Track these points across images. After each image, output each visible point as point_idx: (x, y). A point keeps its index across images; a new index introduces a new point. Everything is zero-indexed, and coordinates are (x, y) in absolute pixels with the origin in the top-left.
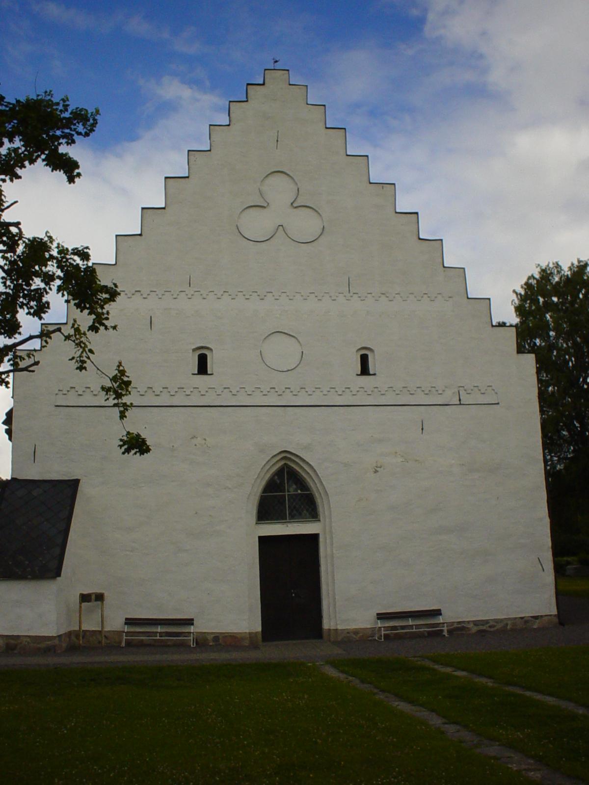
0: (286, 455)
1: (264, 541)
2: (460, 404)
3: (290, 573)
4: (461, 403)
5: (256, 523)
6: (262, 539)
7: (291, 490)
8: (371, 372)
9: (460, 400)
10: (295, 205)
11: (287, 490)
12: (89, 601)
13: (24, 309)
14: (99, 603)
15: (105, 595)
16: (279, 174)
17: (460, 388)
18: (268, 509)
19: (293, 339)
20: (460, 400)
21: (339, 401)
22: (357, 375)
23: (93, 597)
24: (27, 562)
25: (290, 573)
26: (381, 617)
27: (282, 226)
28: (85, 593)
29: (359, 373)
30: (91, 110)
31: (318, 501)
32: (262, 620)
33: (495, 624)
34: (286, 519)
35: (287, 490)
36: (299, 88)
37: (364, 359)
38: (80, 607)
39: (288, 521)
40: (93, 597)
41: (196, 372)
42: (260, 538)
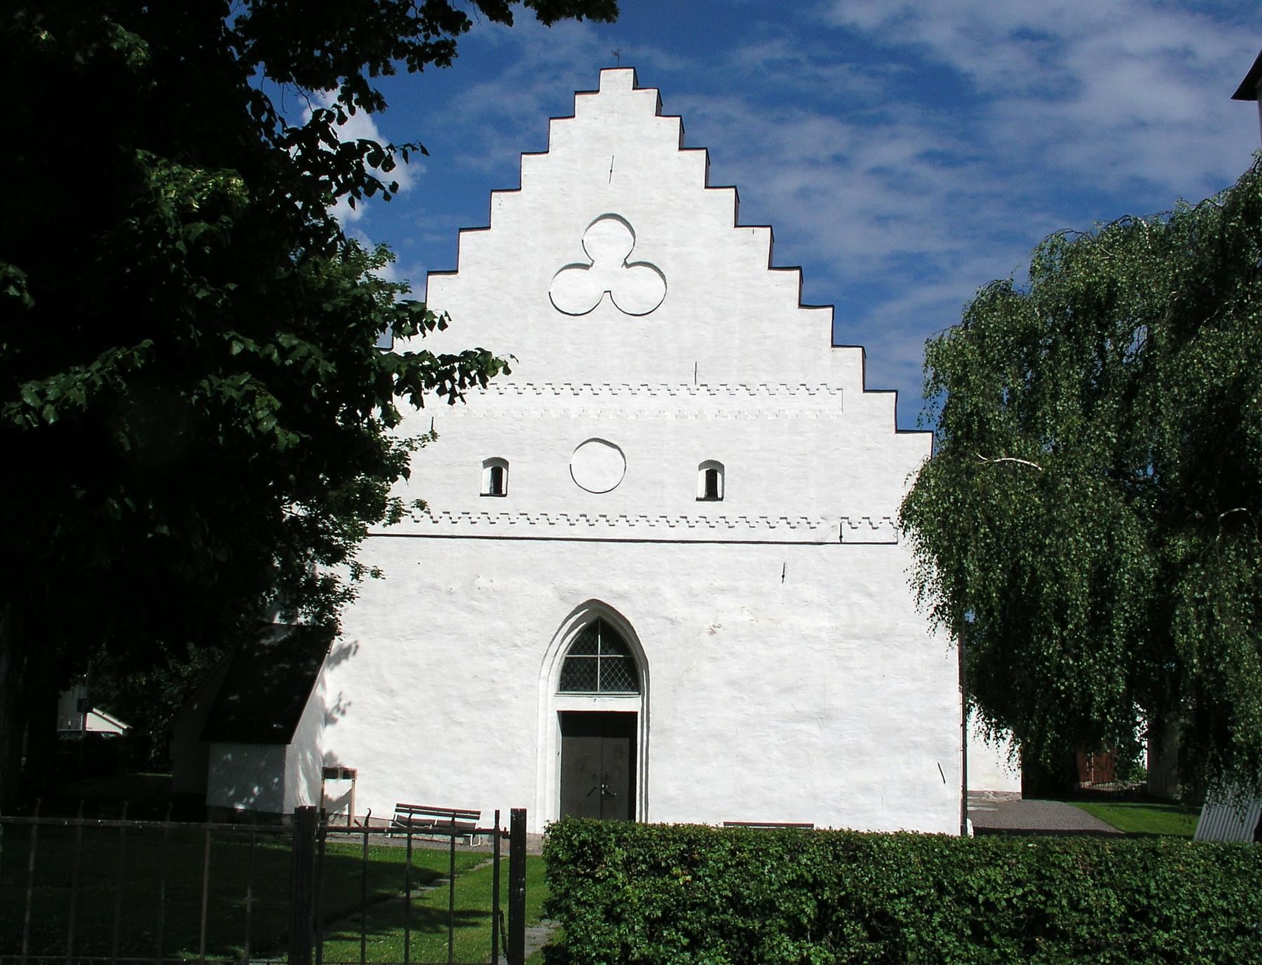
3: (601, 753)
10: (629, 261)
11: (603, 648)
25: (601, 753)
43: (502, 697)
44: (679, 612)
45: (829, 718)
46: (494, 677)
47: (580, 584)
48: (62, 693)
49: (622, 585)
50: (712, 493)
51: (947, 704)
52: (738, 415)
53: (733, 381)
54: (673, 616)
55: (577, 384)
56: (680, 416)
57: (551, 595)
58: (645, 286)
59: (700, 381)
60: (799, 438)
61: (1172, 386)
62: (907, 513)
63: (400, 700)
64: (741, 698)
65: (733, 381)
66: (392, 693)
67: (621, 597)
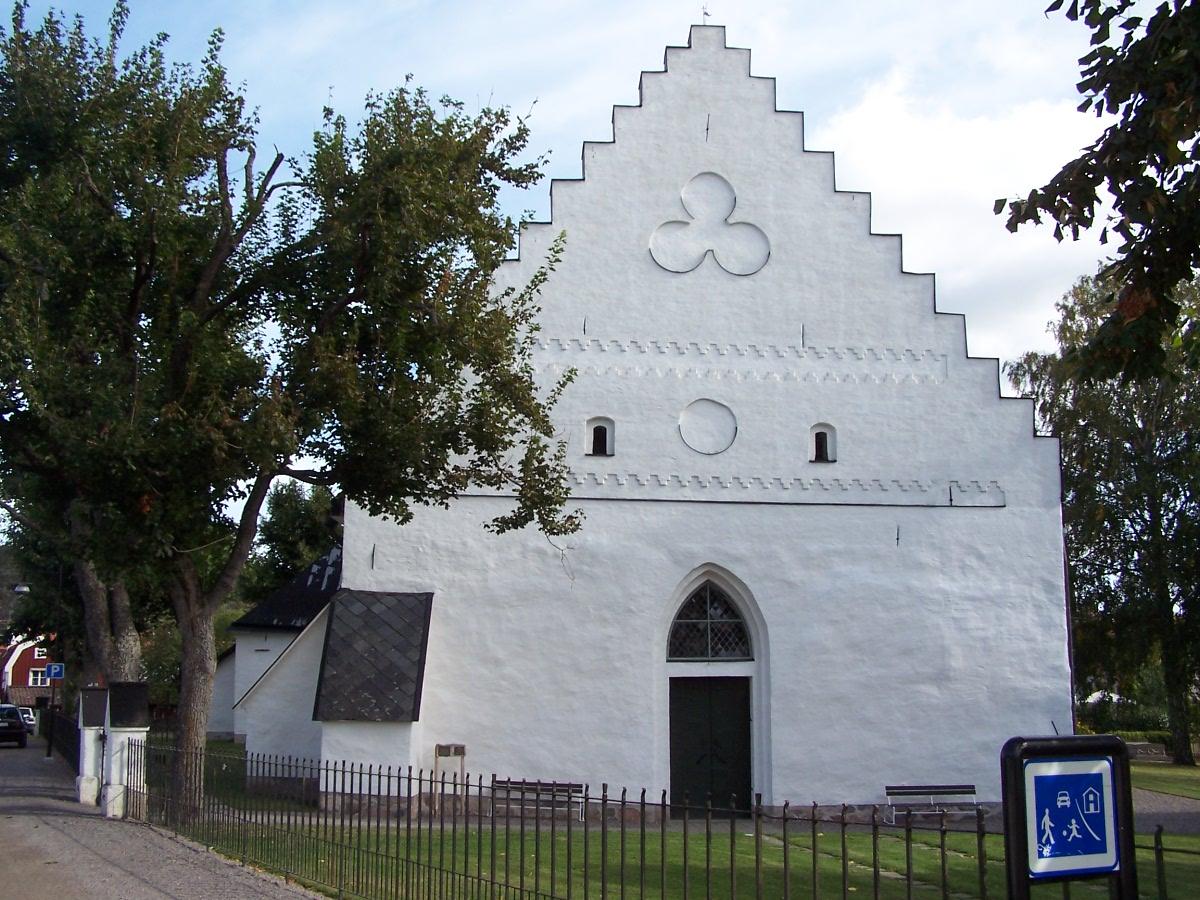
0: (710, 568)
1: (675, 683)
2: (951, 506)
3: (713, 733)
4: (954, 504)
5: (668, 661)
6: (674, 681)
7: (715, 613)
8: (830, 458)
9: (951, 500)
10: (731, 221)
11: (712, 618)
12: (448, 755)
13: (1037, 221)
14: (459, 758)
15: (467, 748)
16: (713, 179)
17: (952, 484)
18: (682, 643)
19: (724, 409)
20: (951, 500)
21: (785, 497)
22: (811, 461)
23: (453, 750)
24: (374, 701)
25: (713, 733)
26: (891, 791)
27: (712, 251)
28: (443, 743)
29: (814, 459)
30: (319, 124)
31: (753, 632)
32: (1036, 790)
33: (988, 809)
34: (707, 656)
35: (712, 618)
36: (740, 53)
37: (821, 440)
38: (436, 762)
39: (710, 658)
40: (453, 750)
41: (591, 452)
42: (672, 680)
43: (618, 665)
44: (797, 574)
45: (948, 679)
46: (608, 645)
47: (696, 548)
48: (1059, 356)
49: (742, 548)
50: (821, 456)
51: (1057, 663)
52: (846, 378)
53: (840, 344)
54: (792, 579)
55: (683, 343)
56: (787, 377)
57: (664, 558)
58: (739, 249)
59: (807, 342)
60: (907, 403)
61: (95, 324)
62: (1157, 9)
63: (508, 670)
64: (863, 661)
65: (840, 344)
66: (497, 662)
67: (738, 560)
